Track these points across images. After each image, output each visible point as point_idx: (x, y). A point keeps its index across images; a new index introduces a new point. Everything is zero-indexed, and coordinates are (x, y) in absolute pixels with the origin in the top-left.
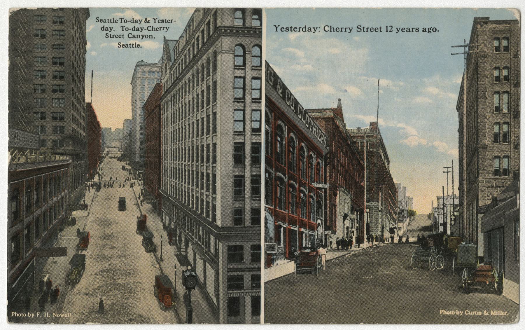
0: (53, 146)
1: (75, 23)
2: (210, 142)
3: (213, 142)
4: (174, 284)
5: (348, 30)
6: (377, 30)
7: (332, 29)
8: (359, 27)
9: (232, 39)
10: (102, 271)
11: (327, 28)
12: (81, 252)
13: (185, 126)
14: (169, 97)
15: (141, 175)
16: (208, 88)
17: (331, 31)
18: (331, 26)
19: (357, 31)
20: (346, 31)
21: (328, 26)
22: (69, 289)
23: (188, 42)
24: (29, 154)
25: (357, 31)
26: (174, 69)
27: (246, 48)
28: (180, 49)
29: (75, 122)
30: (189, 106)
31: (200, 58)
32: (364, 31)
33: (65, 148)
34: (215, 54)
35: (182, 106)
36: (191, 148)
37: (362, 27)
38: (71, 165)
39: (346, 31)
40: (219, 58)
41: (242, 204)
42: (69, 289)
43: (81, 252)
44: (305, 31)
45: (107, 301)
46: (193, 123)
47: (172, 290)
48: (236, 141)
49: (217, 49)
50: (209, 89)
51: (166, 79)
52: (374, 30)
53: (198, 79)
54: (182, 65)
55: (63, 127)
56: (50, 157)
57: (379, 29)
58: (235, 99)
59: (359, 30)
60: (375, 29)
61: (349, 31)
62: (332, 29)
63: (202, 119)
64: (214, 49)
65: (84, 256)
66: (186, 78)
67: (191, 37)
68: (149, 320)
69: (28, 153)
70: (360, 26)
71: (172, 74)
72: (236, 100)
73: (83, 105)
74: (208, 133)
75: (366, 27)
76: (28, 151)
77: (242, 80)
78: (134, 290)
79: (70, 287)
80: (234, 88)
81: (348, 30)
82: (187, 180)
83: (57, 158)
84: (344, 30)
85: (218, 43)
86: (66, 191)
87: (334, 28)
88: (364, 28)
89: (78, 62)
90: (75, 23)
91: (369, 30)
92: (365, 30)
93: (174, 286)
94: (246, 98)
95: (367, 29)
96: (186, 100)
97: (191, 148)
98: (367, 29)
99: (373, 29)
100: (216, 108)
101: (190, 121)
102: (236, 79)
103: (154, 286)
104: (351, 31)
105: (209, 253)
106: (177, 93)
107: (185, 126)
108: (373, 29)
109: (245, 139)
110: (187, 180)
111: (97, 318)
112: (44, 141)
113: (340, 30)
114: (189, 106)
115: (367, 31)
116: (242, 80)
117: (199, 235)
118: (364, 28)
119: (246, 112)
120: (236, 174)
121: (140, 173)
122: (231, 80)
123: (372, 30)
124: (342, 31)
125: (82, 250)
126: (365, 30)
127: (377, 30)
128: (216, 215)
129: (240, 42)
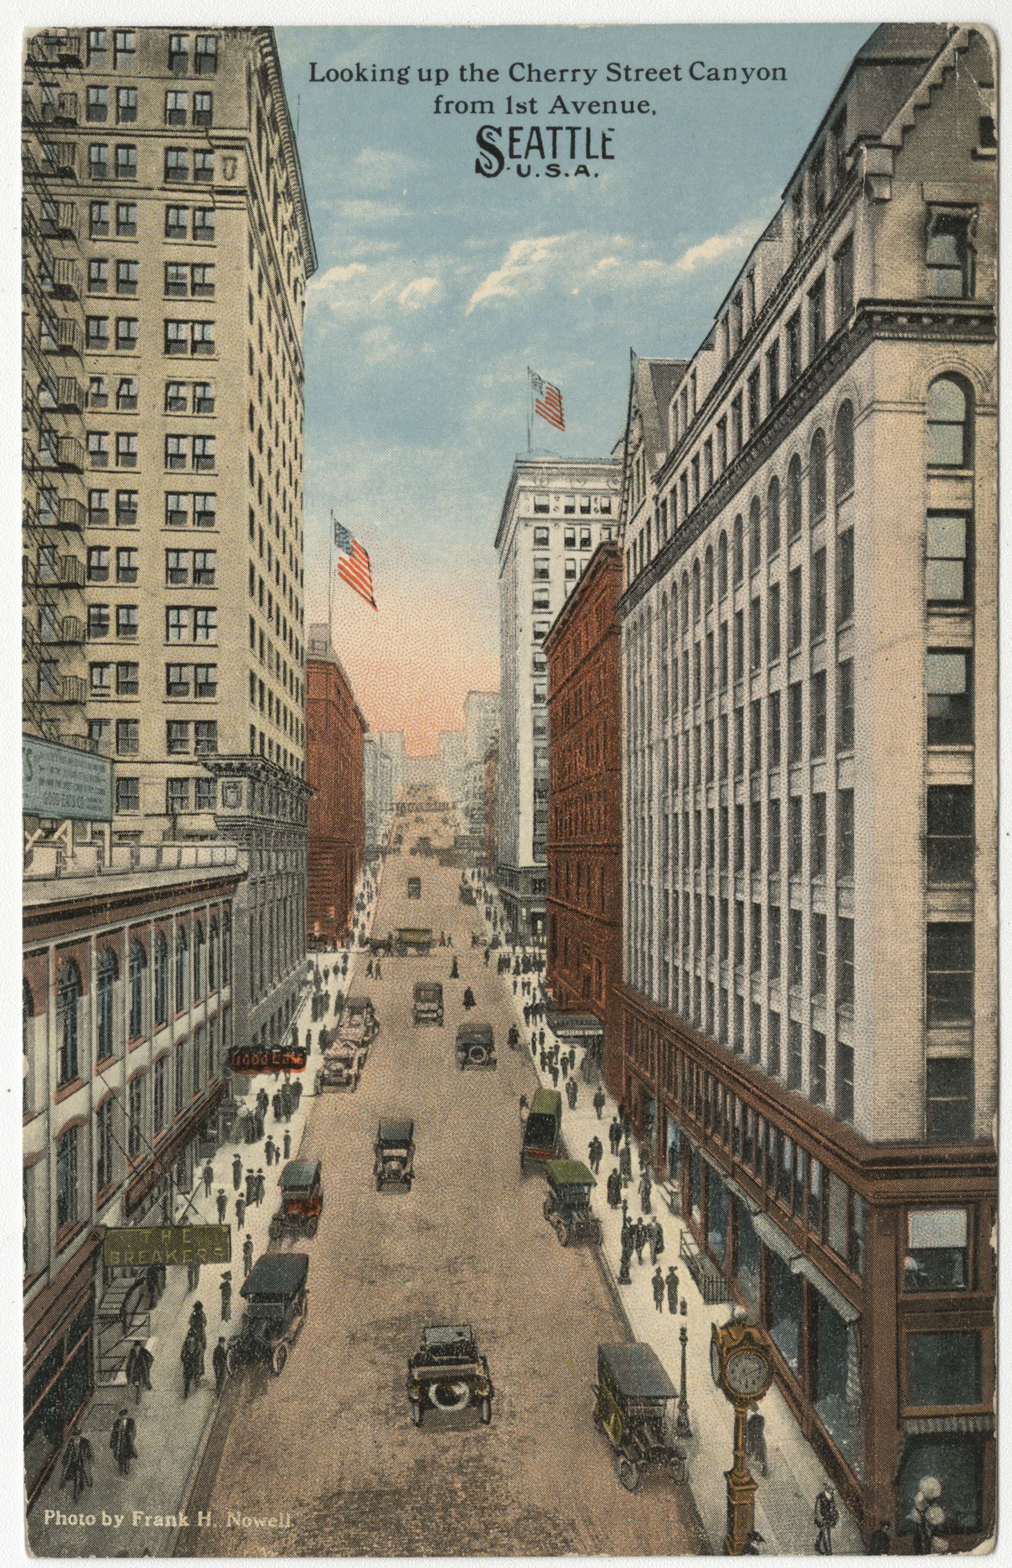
0: (170, 800)
1: (260, 292)
2: (827, 787)
3: (843, 786)
4: (675, 1378)
5: (582, 77)
6: (665, 76)
7: (534, 75)
8: (613, 67)
9: (913, 350)
10: (378, 1325)
11: (518, 72)
12: (291, 1246)
13: (724, 718)
14: (653, 597)
15: (540, 923)
16: (818, 558)
17: (530, 80)
18: (530, 66)
19: (609, 79)
20: (574, 80)
21: (522, 65)
22: (242, 1400)
23: (730, 368)
24: (68, 840)
25: (609, 79)
26: (676, 479)
27: (977, 388)
28: (700, 399)
29: (261, 704)
30: (740, 635)
31: (785, 432)
32: (627, 79)
33: (220, 810)
34: (845, 413)
35: (710, 636)
36: (747, 810)
37: (623, 66)
38: (243, 885)
39: (574, 80)
40: (860, 435)
41: (960, 1043)
42: (242, 1400)
43: (291, 1246)
44: (438, 71)
45: (397, 1450)
46: (756, 705)
47: (672, 1407)
48: (935, 781)
49: (855, 399)
50: (824, 560)
51: (640, 523)
52: (657, 75)
53: (775, 520)
54: (710, 462)
55: (211, 723)
56: (159, 850)
57: (673, 72)
58: (931, 603)
59: (615, 76)
60: (661, 73)
61: (586, 80)
62: (534, 75)
63: (795, 689)
64: (845, 396)
65: (305, 1259)
66: (726, 519)
67: (745, 343)
68: (574, 1529)
69: (65, 833)
70: (618, 65)
71: (664, 504)
72: (935, 607)
73: (297, 634)
74: (818, 749)
75: (634, 67)
76: (68, 824)
77: (958, 525)
78: (511, 1404)
79: (245, 1387)
80: (926, 559)
81: (582, 77)
82: (717, 942)
83: (189, 856)
84: (568, 76)
85: (859, 370)
86: (225, 993)
87: (538, 72)
88: (627, 69)
89: (270, 455)
90: (260, 292)
91: (642, 75)
92: (632, 74)
93: (678, 1391)
94: (978, 601)
95: (637, 71)
96: (724, 606)
97: (747, 810)
98: (637, 71)
99: (655, 72)
100: (851, 646)
101: (740, 699)
102: (934, 522)
103: (593, 1387)
104: (590, 78)
105: (826, 1250)
106: (685, 582)
107: (724, 718)
108: (655, 72)
109: (972, 774)
110: (717, 942)
111: (354, 1523)
112: (130, 782)
113: (558, 76)
114: (740, 635)
115: (637, 79)
116: (958, 525)
117: (767, 1156)
118: (627, 69)
119: (978, 661)
120: (936, 918)
121: (534, 917)
122: (913, 523)
123: (652, 76)
124: (562, 80)
125: (295, 1236)
126: (632, 74)
127: (665, 76)
128: (852, 1088)
129: (954, 366)
